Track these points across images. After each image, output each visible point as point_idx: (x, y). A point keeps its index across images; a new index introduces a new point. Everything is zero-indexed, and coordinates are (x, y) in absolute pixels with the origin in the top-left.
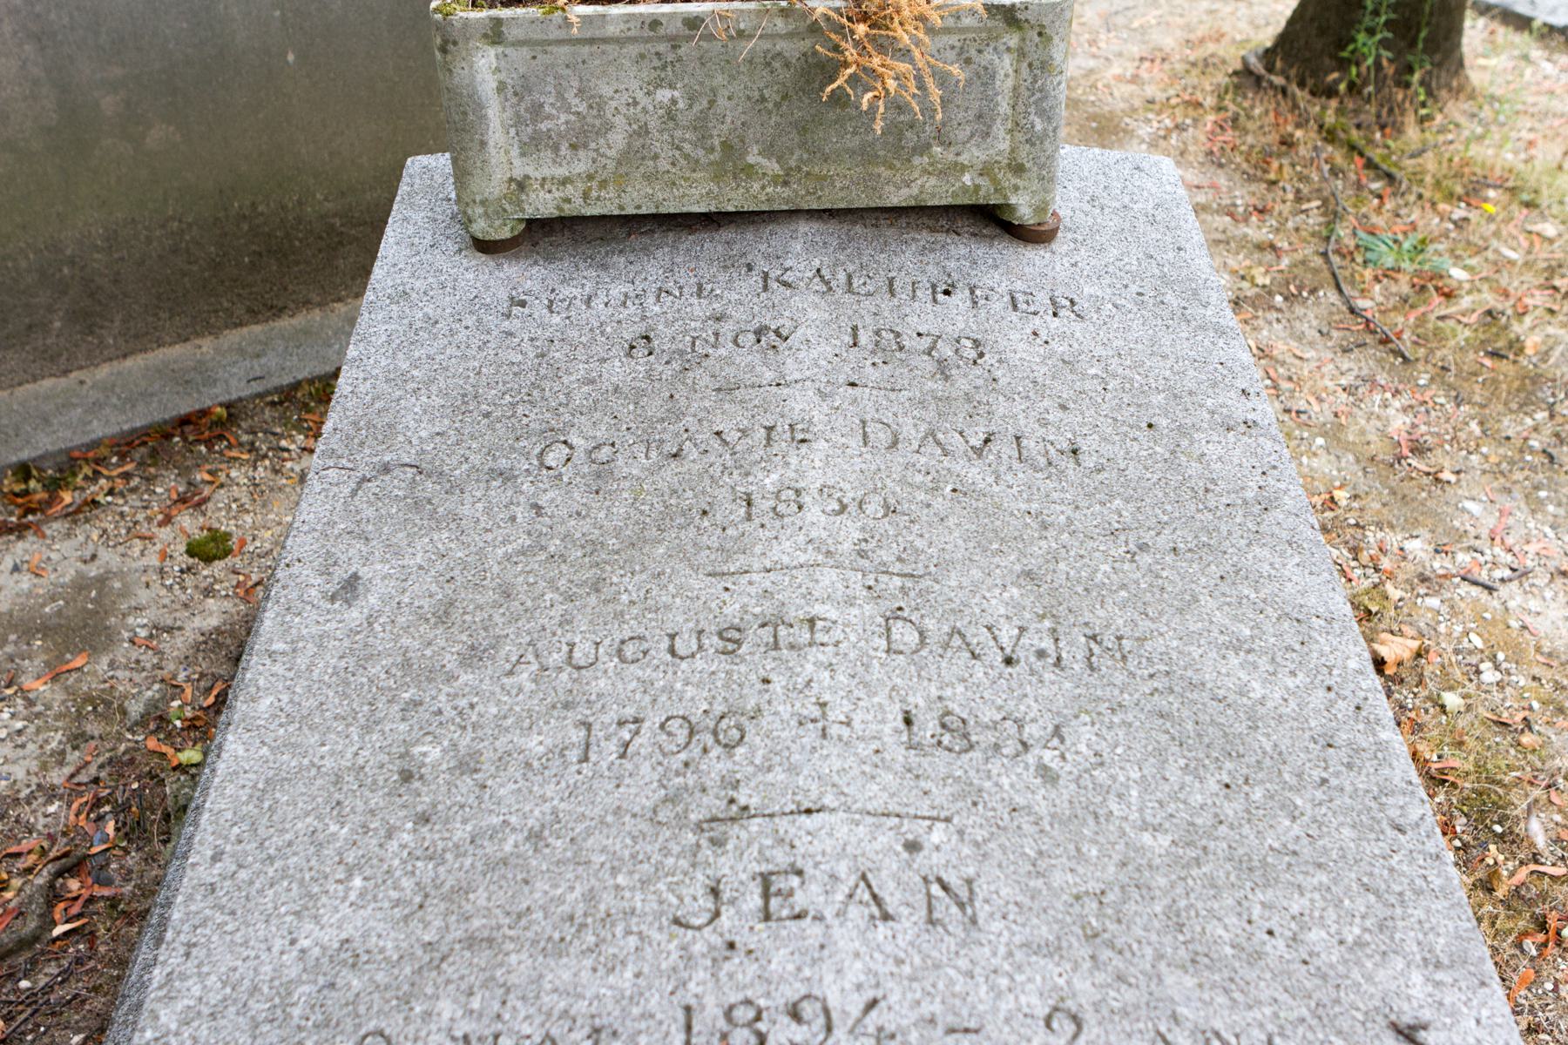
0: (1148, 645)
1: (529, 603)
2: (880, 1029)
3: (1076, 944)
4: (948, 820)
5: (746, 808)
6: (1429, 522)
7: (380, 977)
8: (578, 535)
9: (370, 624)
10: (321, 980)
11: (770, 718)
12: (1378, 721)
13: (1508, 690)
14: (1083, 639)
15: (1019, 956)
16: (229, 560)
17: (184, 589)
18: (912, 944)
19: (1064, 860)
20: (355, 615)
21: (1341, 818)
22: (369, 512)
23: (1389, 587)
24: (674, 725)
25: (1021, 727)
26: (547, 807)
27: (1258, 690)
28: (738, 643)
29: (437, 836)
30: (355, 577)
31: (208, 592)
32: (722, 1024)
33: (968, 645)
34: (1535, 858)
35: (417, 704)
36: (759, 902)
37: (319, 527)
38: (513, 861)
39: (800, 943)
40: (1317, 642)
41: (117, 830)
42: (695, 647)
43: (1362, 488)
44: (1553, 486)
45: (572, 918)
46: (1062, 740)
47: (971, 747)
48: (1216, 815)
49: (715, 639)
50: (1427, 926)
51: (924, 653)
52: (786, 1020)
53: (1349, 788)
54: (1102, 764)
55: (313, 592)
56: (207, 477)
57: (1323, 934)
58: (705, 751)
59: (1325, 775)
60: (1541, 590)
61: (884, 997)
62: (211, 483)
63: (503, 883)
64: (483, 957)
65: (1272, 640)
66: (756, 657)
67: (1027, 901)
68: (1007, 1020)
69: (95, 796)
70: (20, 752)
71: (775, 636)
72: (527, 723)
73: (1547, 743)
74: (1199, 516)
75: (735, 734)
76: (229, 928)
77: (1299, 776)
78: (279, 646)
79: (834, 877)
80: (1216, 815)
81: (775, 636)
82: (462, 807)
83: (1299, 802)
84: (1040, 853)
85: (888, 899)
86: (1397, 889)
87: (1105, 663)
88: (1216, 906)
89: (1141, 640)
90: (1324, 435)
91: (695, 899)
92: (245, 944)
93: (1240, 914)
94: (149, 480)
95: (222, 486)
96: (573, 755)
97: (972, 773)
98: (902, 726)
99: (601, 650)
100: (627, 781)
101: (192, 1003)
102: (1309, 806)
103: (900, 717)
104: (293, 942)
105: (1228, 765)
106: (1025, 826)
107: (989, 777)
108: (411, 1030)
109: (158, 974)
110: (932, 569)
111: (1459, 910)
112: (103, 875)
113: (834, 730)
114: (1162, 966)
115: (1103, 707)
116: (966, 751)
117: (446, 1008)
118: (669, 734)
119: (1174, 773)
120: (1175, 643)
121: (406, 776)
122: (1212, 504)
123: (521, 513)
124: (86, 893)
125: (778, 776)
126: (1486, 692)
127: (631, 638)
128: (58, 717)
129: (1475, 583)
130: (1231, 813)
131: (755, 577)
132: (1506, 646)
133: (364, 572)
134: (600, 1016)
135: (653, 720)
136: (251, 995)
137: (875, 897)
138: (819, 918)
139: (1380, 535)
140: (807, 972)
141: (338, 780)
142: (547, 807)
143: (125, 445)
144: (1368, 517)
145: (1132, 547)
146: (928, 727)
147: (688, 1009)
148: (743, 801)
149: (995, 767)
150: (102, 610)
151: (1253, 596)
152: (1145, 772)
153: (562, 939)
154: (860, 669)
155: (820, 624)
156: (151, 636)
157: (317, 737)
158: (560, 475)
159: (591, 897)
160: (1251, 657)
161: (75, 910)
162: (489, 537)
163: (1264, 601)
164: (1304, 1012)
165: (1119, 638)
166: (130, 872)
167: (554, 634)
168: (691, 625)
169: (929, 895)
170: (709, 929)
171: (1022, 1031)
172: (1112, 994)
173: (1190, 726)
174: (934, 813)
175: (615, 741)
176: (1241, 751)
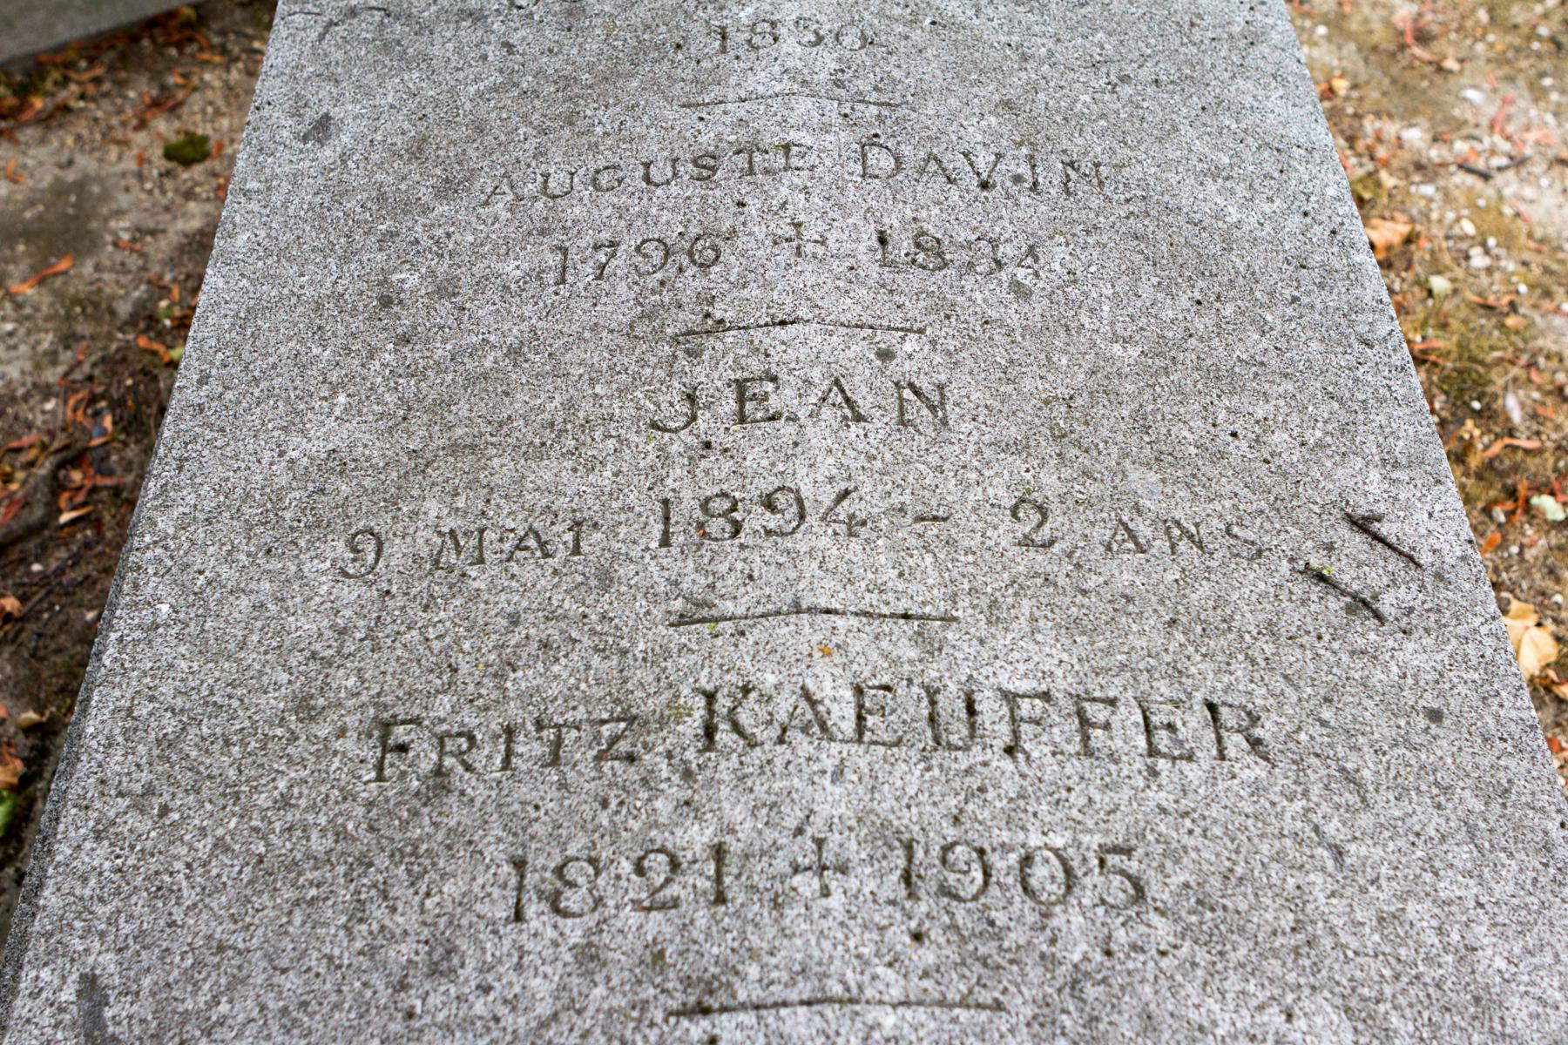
0: (1126, 172)
1: (503, 138)
2: (852, 517)
3: (1043, 443)
4: (921, 331)
5: (721, 321)
6: (1429, 111)
7: (368, 482)
8: (550, 71)
9: (344, 162)
10: (311, 486)
11: (745, 239)
12: (1352, 245)
13: (1497, 276)
14: (1060, 166)
15: (988, 453)
16: (208, 164)
17: (164, 192)
18: (883, 441)
19: (1035, 368)
20: (328, 154)
21: (1310, 333)
22: (339, 55)
23: (1384, 175)
24: (650, 248)
25: (995, 248)
26: (525, 326)
27: (1234, 214)
28: (714, 169)
29: (418, 355)
30: (327, 117)
31: (189, 195)
32: (698, 514)
33: (944, 170)
34: (1511, 432)
35: (394, 235)
36: (735, 406)
37: (287, 71)
38: (493, 375)
39: (774, 441)
40: (1296, 170)
41: (115, 423)
42: (670, 175)
43: (1363, 77)
44: (1557, 73)
45: (552, 425)
46: (1036, 260)
47: (946, 265)
48: (1186, 329)
49: (690, 166)
50: (1388, 430)
51: (900, 177)
52: (760, 510)
53: (1319, 306)
54: (1075, 282)
55: (285, 133)
56: (180, 80)
57: (1286, 436)
58: (681, 270)
59: (1296, 293)
60: (1538, 178)
61: (856, 489)
62: (183, 86)
63: (484, 395)
64: (467, 462)
65: (1251, 168)
66: (731, 182)
67: (997, 405)
68: (974, 510)
69: (91, 392)
70: (13, 354)
71: (750, 163)
72: (502, 251)
73: (1531, 324)
74: (1183, 49)
75: (711, 254)
76: (219, 444)
77: (1271, 294)
78: (253, 185)
79: (808, 382)
80: (1186, 329)
81: (750, 163)
82: (442, 328)
83: (1269, 318)
84: (1012, 361)
85: (860, 402)
86: (1361, 397)
87: (1082, 189)
88: (1182, 411)
89: (1119, 167)
90: (1327, 23)
91: (672, 405)
92: (236, 457)
93: (1205, 418)
94: (121, 84)
95: (195, 89)
96: (550, 278)
97: (946, 289)
98: (877, 245)
99: (576, 179)
100: (604, 300)
101: (187, 510)
102: (1279, 321)
103: (874, 237)
104: (282, 454)
105: (1201, 283)
106: (996, 337)
107: (963, 293)
108: (399, 527)
109: (152, 486)
110: (910, 98)
111: (1419, 417)
112: (104, 466)
113: (809, 248)
114: (1127, 463)
115: (1078, 229)
116: (940, 269)
117: (432, 507)
118: (645, 256)
119: (1146, 291)
120: (1153, 170)
121: (386, 302)
122: (1197, 38)
123: (493, 52)
124: (88, 484)
125: (754, 292)
126: (1475, 276)
127: (606, 168)
128: (48, 319)
129: (1471, 171)
130: (1202, 327)
131: (730, 107)
132: (1498, 232)
133: (336, 112)
134: (581, 510)
135: (629, 243)
136: (244, 502)
137: (847, 400)
138: (793, 419)
139: (1378, 124)
140: (781, 467)
141: (319, 307)
142: (525, 326)
143: (93, 48)
144: (1367, 106)
145: (1113, 78)
146: (903, 245)
147: (666, 502)
148: (718, 315)
149: (969, 282)
150: (84, 211)
151: (1234, 126)
152: (1118, 289)
153: (543, 444)
154: (834, 191)
155: (795, 150)
156: (134, 240)
157: (295, 268)
158: (532, 14)
159: (570, 406)
160: (1228, 184)
161: (80, 498)
162: (461, 75)
163: (1245, 131)
164: (1263, 504)
165: (1097, 165)
166: (130, 463)
167: (529, 166)
168: (666, 154)
169: (901, 398)
170: (687, 430)
171: (989, 519)
172: (1077, 487)
173: (1164, 248)
174: (908, 325)
175: (591, 263)
176: (1214, 271)
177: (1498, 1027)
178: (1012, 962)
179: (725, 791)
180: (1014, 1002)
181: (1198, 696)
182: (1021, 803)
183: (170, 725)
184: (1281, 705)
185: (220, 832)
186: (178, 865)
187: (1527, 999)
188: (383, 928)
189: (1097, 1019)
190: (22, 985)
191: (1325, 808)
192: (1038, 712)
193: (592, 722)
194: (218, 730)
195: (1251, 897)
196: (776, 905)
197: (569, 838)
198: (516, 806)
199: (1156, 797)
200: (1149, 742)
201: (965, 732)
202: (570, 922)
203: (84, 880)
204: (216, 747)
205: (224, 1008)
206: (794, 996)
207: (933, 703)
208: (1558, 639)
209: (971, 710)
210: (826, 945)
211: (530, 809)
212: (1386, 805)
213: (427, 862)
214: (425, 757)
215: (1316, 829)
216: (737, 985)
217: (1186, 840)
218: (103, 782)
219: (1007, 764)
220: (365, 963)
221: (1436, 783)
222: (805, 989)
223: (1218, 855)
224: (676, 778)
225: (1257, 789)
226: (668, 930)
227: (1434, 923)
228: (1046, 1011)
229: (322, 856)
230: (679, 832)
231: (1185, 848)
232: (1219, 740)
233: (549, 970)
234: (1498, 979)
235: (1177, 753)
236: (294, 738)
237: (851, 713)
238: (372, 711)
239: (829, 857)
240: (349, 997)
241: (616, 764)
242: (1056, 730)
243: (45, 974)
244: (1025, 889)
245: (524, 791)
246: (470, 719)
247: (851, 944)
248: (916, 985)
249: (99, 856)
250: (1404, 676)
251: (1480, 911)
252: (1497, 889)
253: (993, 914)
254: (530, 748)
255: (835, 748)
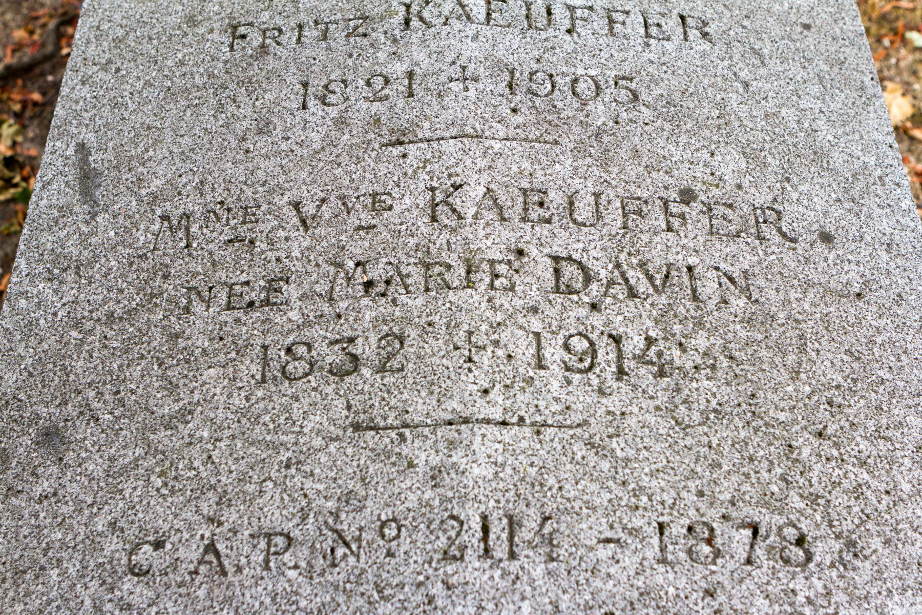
177: (825, 165)
178: (564, 124)
179: (414, 47)
180: (564, 141)
181: (675, 12)
182: (574, 55)
183: (120, 32)
184: (721, 18)
185: (147, 78)
186: (125, 93)
187: (842, 154)
188: (233, 115)
189: (608, 151)
190: (46, 149)
191: (740, 65)
192: (586, 15)
193: (345, 20)
194: (146, 34)
195: (696, 102)
196: (440, 95)
197: (332, 71)
198: (304, 59)
199: (647, 55)
200: (646, 32)
201: (545, 22)
202: (331, 108)
203: (77, 102)
204: (145, 41)
205: (151, 153)
206: (448, 135)
207: (529, 9)
208: (914, 106)
209: (549, 13)
210: (466, 112)
211: (311, 60)
212: (775, 65)
213: (257, 85)
214: (256, 39)
215: (735, 74)
216: (418, 130)
217: (663, 75)
218: (85, 59)
219: (568, 37)
220: (224, 130)
221: (804, 57)
222: (454, 131)
223: (679, 83)
224: (388, 43)
225: (704, 55)
226: (382, 109)
227: (796, 118)
228: (581, 146)
229: (201, 86)
230: (389, 66)
231: (662, 79)
232: (685, 33)
233: (320, 129)
234: (828, 144)
235: (661, 37)
236: (185, 34)
237: (484, 12)
238: (227, 21)
239: (468, 73)
240: (216, 145)
241: (357, 38)
242: (595, 23)
243: (58, 144)
244: (574, 93)
245: (308, 52)
246: (279, 21)
247: (479, 112)
248: (512, 133)
249: (85, 92)
250: (792, 8)
251: (822, 115)
252: (832, 105)
253: (556, 103)
254: (310, 33)
255: (474, 26)
